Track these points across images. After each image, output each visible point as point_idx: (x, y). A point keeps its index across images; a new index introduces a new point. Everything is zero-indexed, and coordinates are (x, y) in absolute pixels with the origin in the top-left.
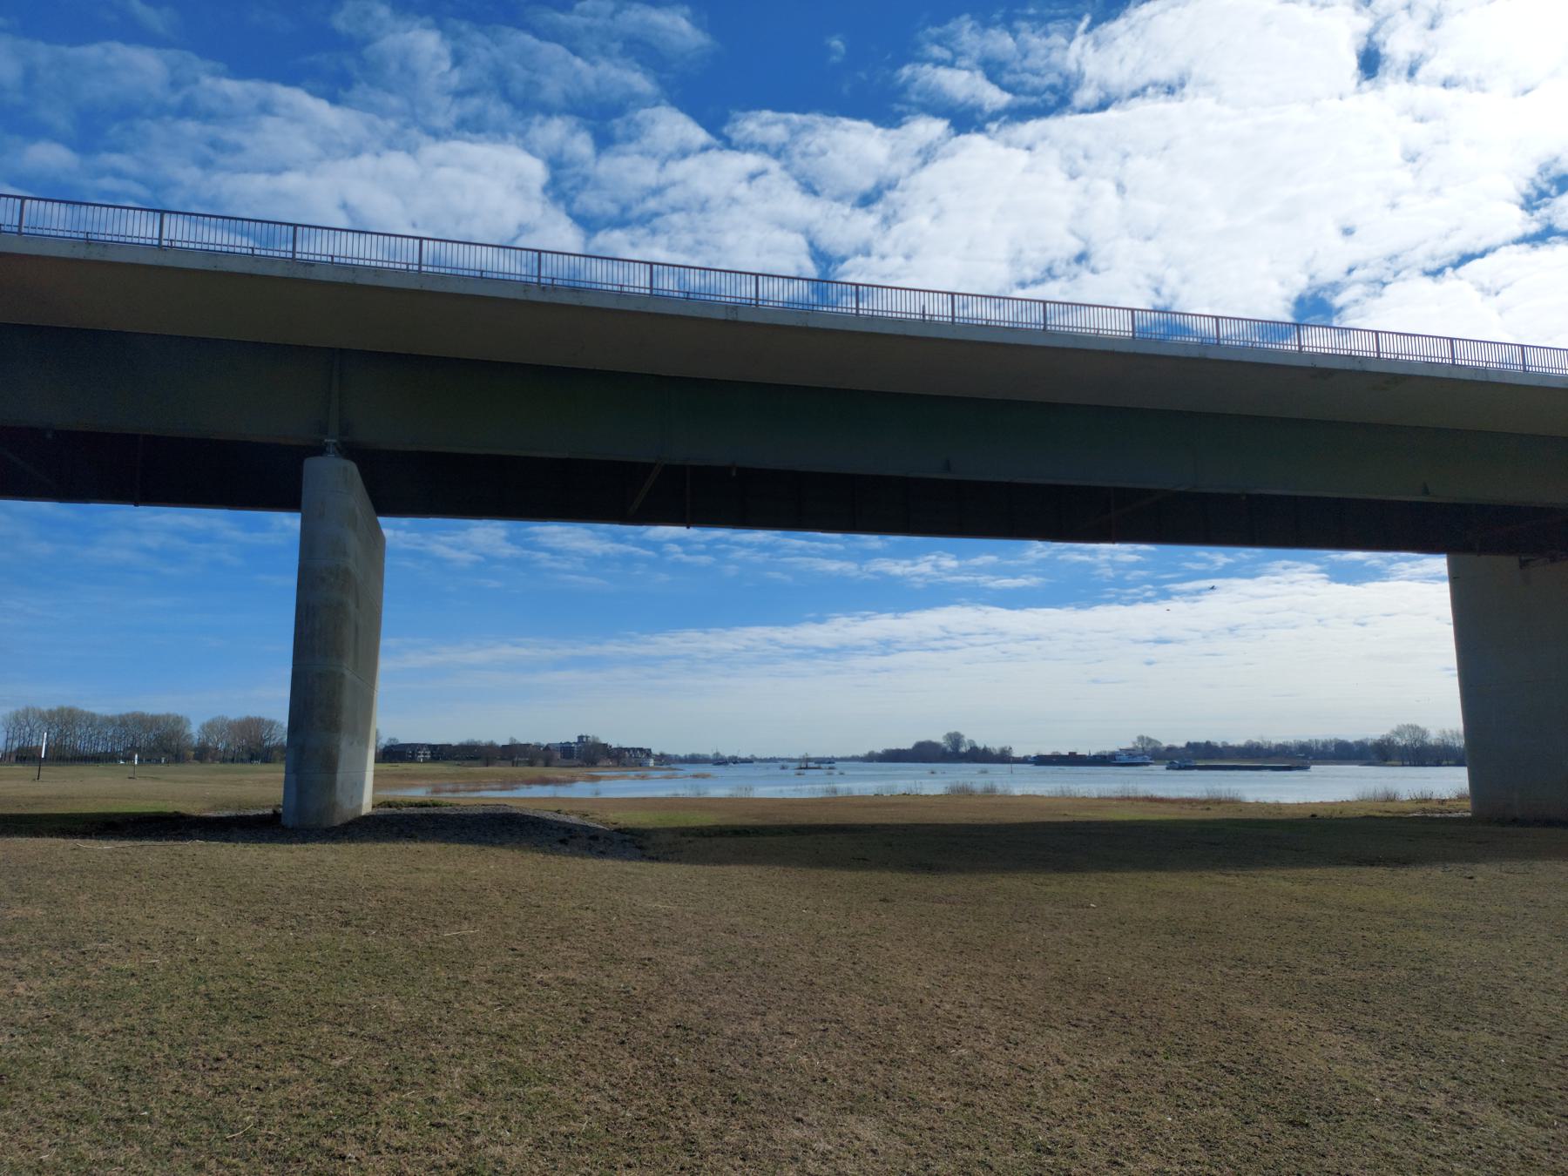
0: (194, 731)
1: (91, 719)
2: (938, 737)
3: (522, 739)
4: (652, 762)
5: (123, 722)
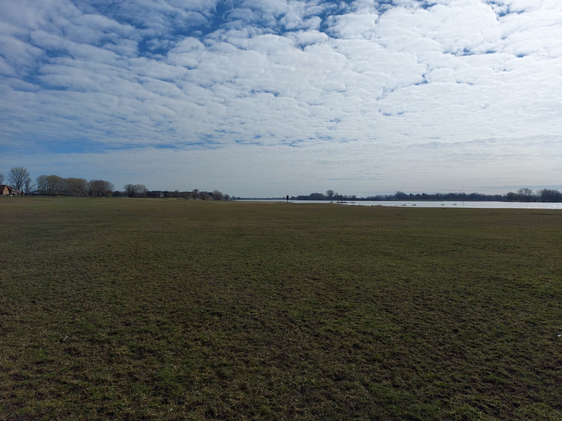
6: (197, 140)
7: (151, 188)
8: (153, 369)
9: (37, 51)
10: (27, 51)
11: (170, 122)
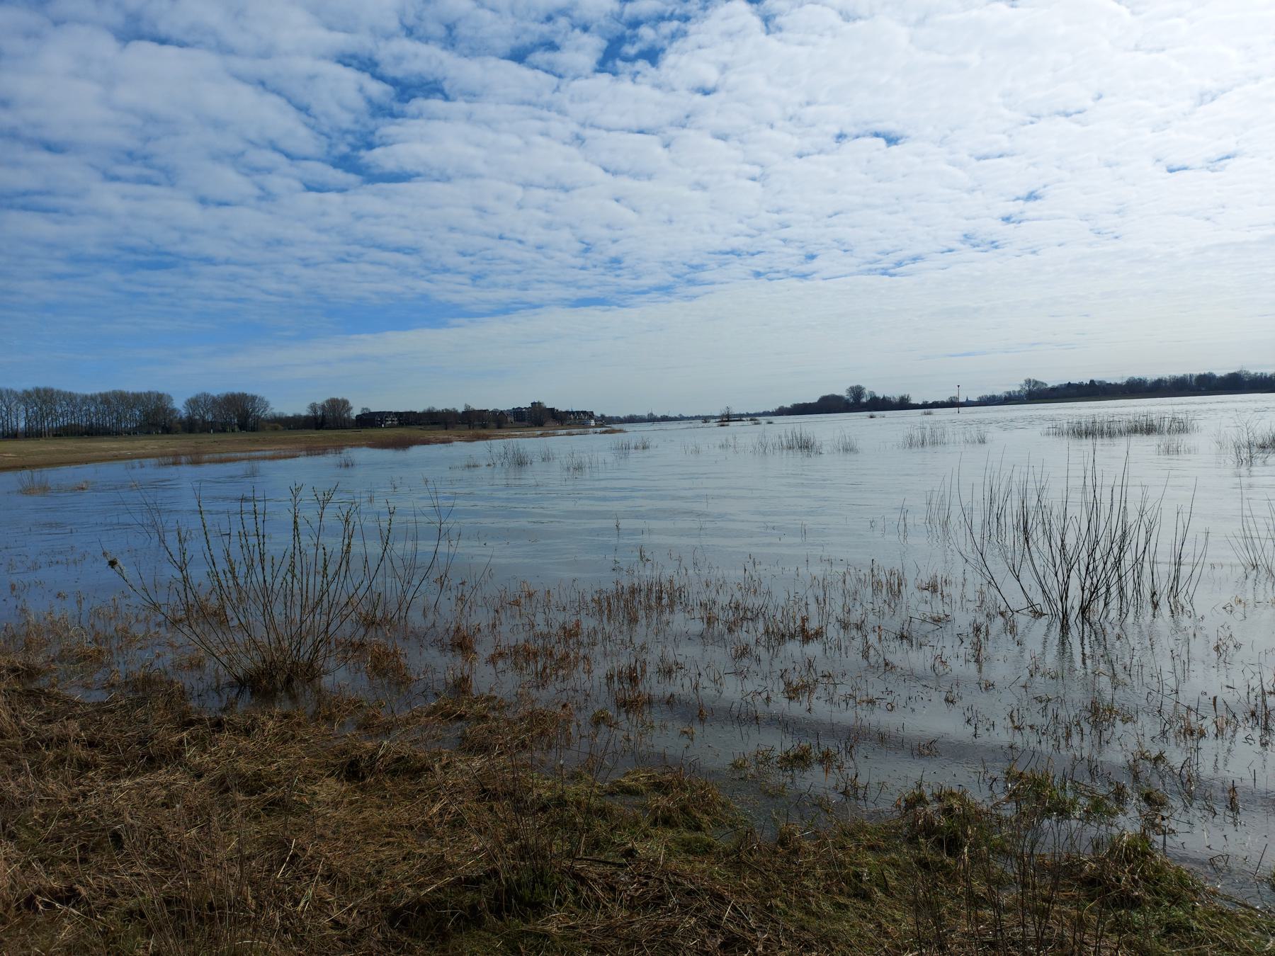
0: (179, 404)
1: (70, 398)
2: (842, 391)
3: (477, 406)
4: (593, 423)
5: (105, 399)
6: (664, 278)
7: (562, 407)
8: (575, 892)
9: (377, 89)
10: (361, 89)
11: (615, 241)
